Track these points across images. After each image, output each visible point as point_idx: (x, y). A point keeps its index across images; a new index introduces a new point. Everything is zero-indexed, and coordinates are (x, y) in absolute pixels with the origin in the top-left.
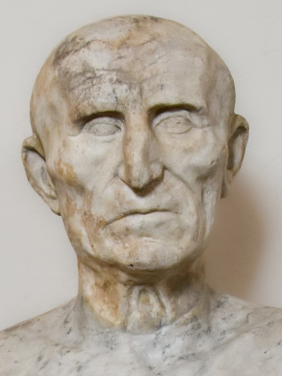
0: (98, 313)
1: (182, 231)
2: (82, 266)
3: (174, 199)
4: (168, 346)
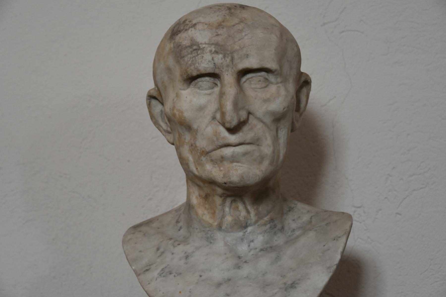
0: (201, 216)
1: (262, 159)
2: (189, 182)
3: (256, 135)
4: (252, 241)
